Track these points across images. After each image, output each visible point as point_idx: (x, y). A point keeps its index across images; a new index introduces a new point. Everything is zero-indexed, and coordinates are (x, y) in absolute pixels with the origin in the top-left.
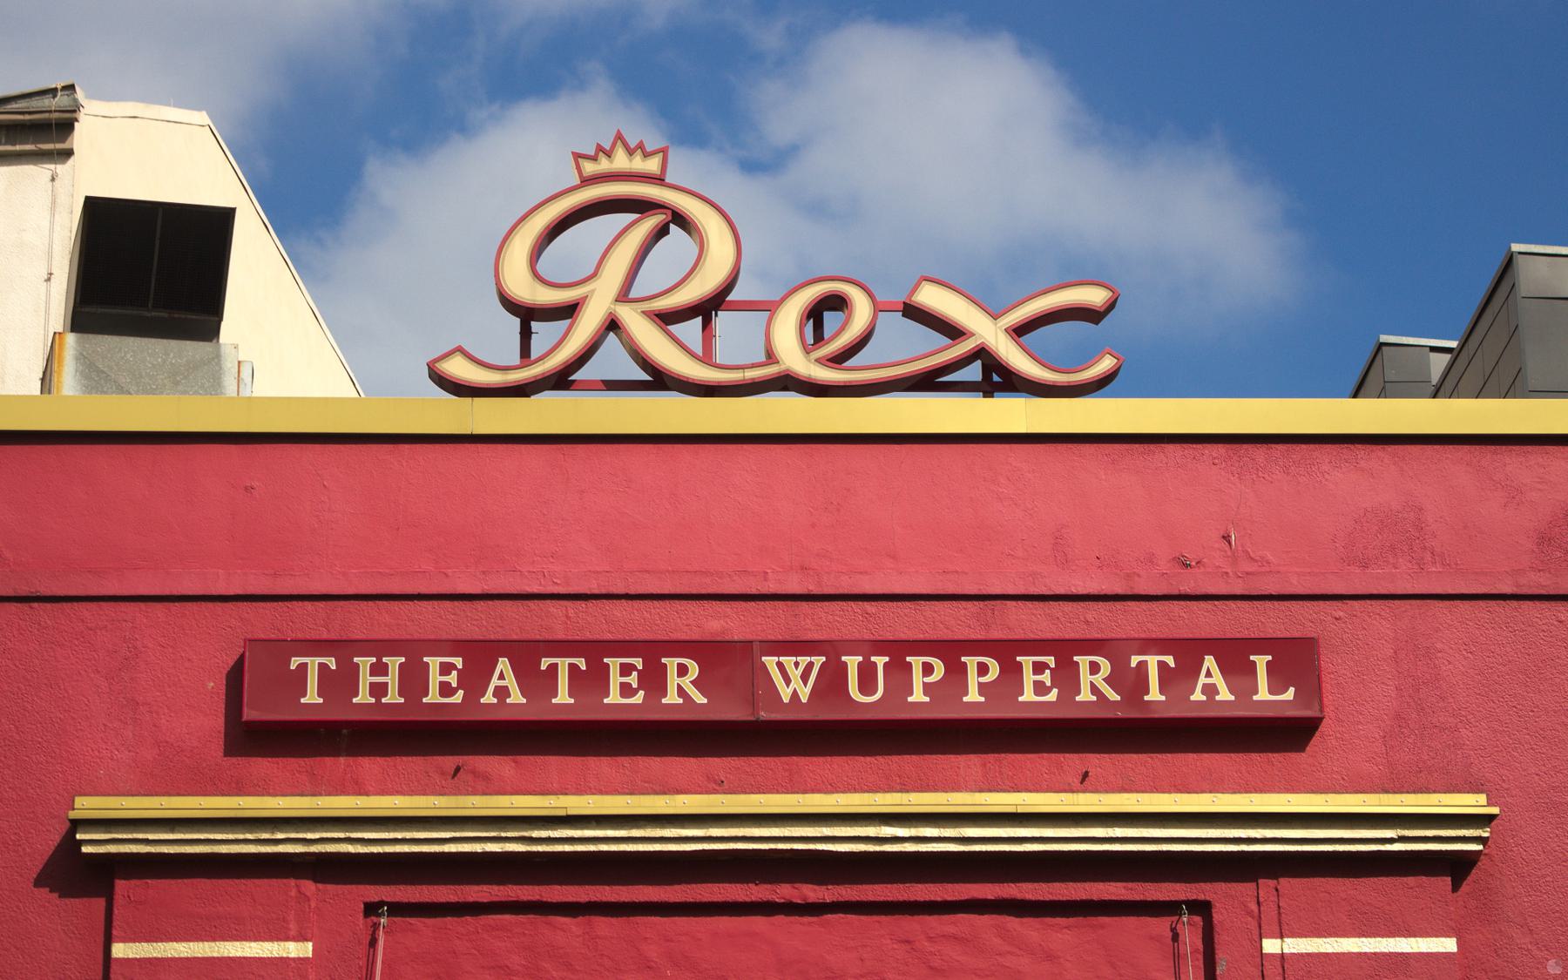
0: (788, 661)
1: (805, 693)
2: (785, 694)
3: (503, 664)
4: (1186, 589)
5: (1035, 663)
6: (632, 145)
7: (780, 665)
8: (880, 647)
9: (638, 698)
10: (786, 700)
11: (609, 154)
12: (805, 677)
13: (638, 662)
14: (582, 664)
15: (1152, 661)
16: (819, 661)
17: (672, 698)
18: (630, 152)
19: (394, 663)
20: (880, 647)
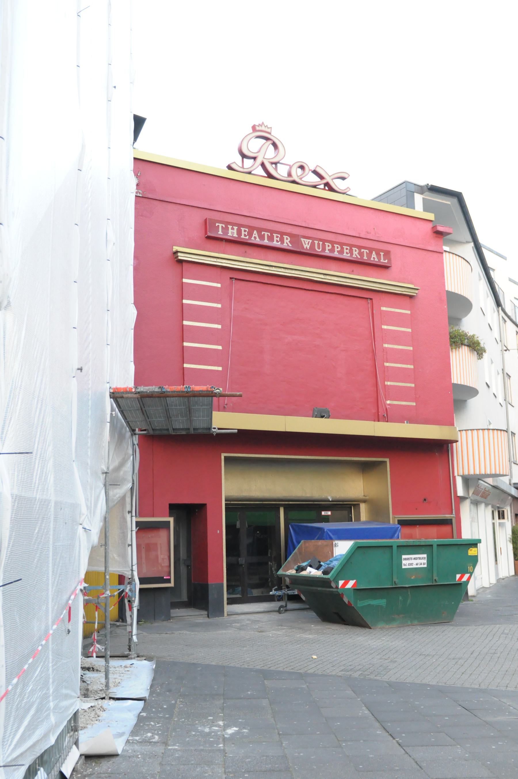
0: (305, 240)
1: (308, 247)
2: (305, 246)
3: (255, 232)
4: (368, 238)
5: (244, 230)
6: (266, 125)
7: (304, 241)
8: (320, 240)
9: (247, 237)
10: (305, 248)
11: (261, 126)
12: (308, 244)
13: (349, 248)
14: (224, 226)
15: (220, 225)
16: (311, 241)
17: (285, 244)
18: (265, 127)
19: (236, 228)
20: (320, 240)
